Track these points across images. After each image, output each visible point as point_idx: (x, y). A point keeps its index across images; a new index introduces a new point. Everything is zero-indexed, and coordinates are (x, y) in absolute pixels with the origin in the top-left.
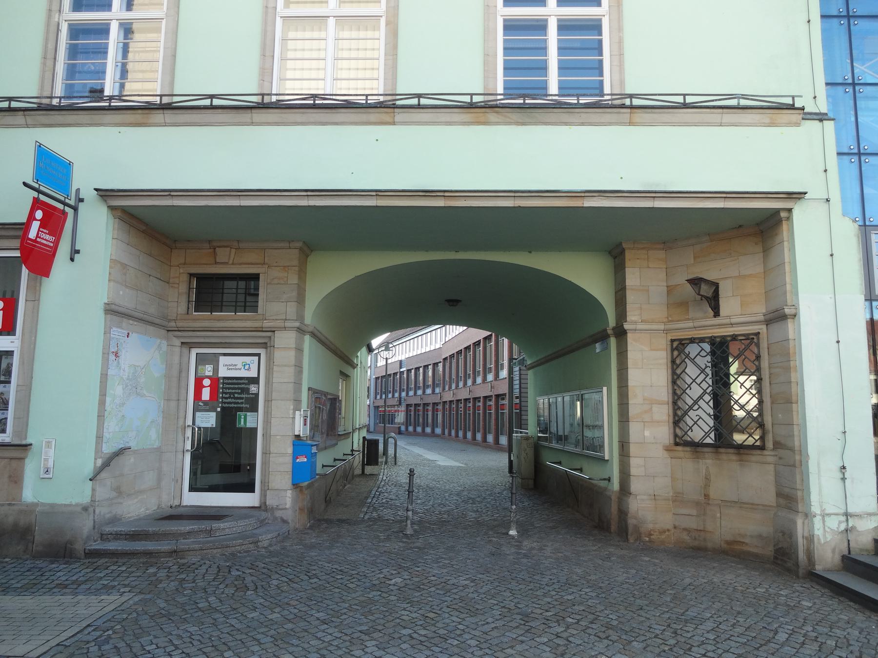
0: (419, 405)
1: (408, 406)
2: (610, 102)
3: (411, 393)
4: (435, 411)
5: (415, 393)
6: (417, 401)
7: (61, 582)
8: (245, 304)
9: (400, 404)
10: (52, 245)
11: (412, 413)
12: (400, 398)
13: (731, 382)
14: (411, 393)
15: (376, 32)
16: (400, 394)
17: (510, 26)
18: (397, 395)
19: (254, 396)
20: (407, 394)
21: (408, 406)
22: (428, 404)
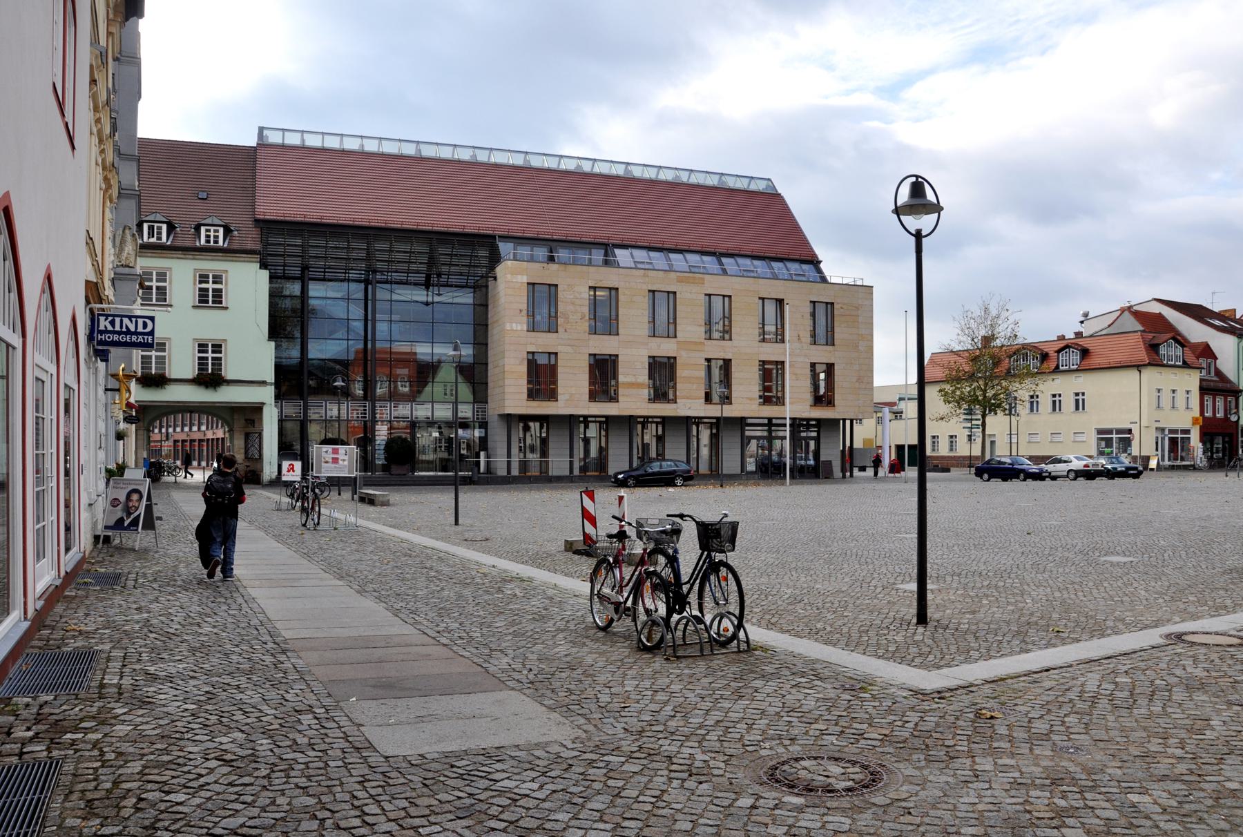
0: (186, 441)
1: (175, 441)
2: (284, 360)
3: (178, 429)
4: (200, 446)
5: (182, 430)
6: (183, 437)
7: (185, 777)
8: (770, 431)
9: (167, 439)
10: (747, 428)
11: (180, 448)
12: (167, 433)
13: (936, 202)
14: (178, 429)
15: (506, 405)
16: (167, 430)
17: (220, 352)
18: (164, 430)
19: (715, 421)
20: (174, 430)
21: (175, 441)
22: (194, 441)
